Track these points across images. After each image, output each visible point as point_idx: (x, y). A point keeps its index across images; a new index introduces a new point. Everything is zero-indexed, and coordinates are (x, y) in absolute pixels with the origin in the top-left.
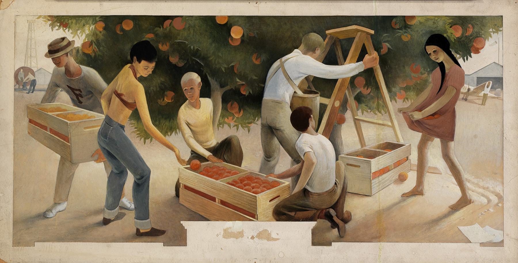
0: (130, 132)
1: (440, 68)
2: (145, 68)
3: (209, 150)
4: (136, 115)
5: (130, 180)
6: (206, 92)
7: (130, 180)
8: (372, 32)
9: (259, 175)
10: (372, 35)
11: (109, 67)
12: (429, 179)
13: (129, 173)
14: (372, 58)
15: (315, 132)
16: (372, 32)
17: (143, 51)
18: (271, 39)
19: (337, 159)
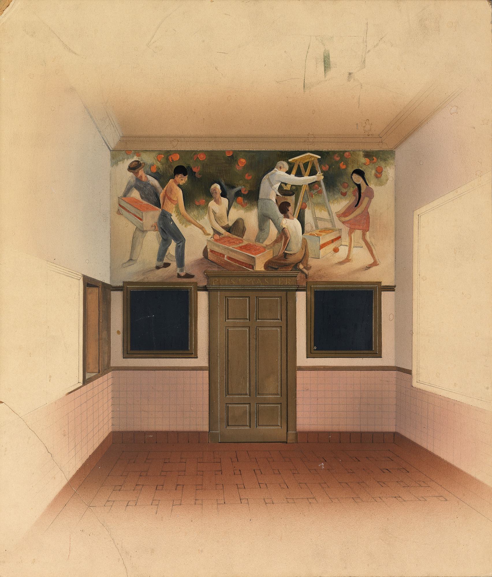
0: (175, 218)
1: (198, 434)
2: (182, 179)
3: (223, 227)
4: (177, 208)
5: (173, 245)
6: (223, 195)
7: (173, 245)
8: (319, 157)
9: (180, 284)
10: (318, 159)
11: (162, 177)
12: (354, 251)
13: (173, 241)
14: (319, 177)
15: (292, 217)
16: (319, 157)
17: (180, 170)
18: (263, 162)
19: (303, 233)
